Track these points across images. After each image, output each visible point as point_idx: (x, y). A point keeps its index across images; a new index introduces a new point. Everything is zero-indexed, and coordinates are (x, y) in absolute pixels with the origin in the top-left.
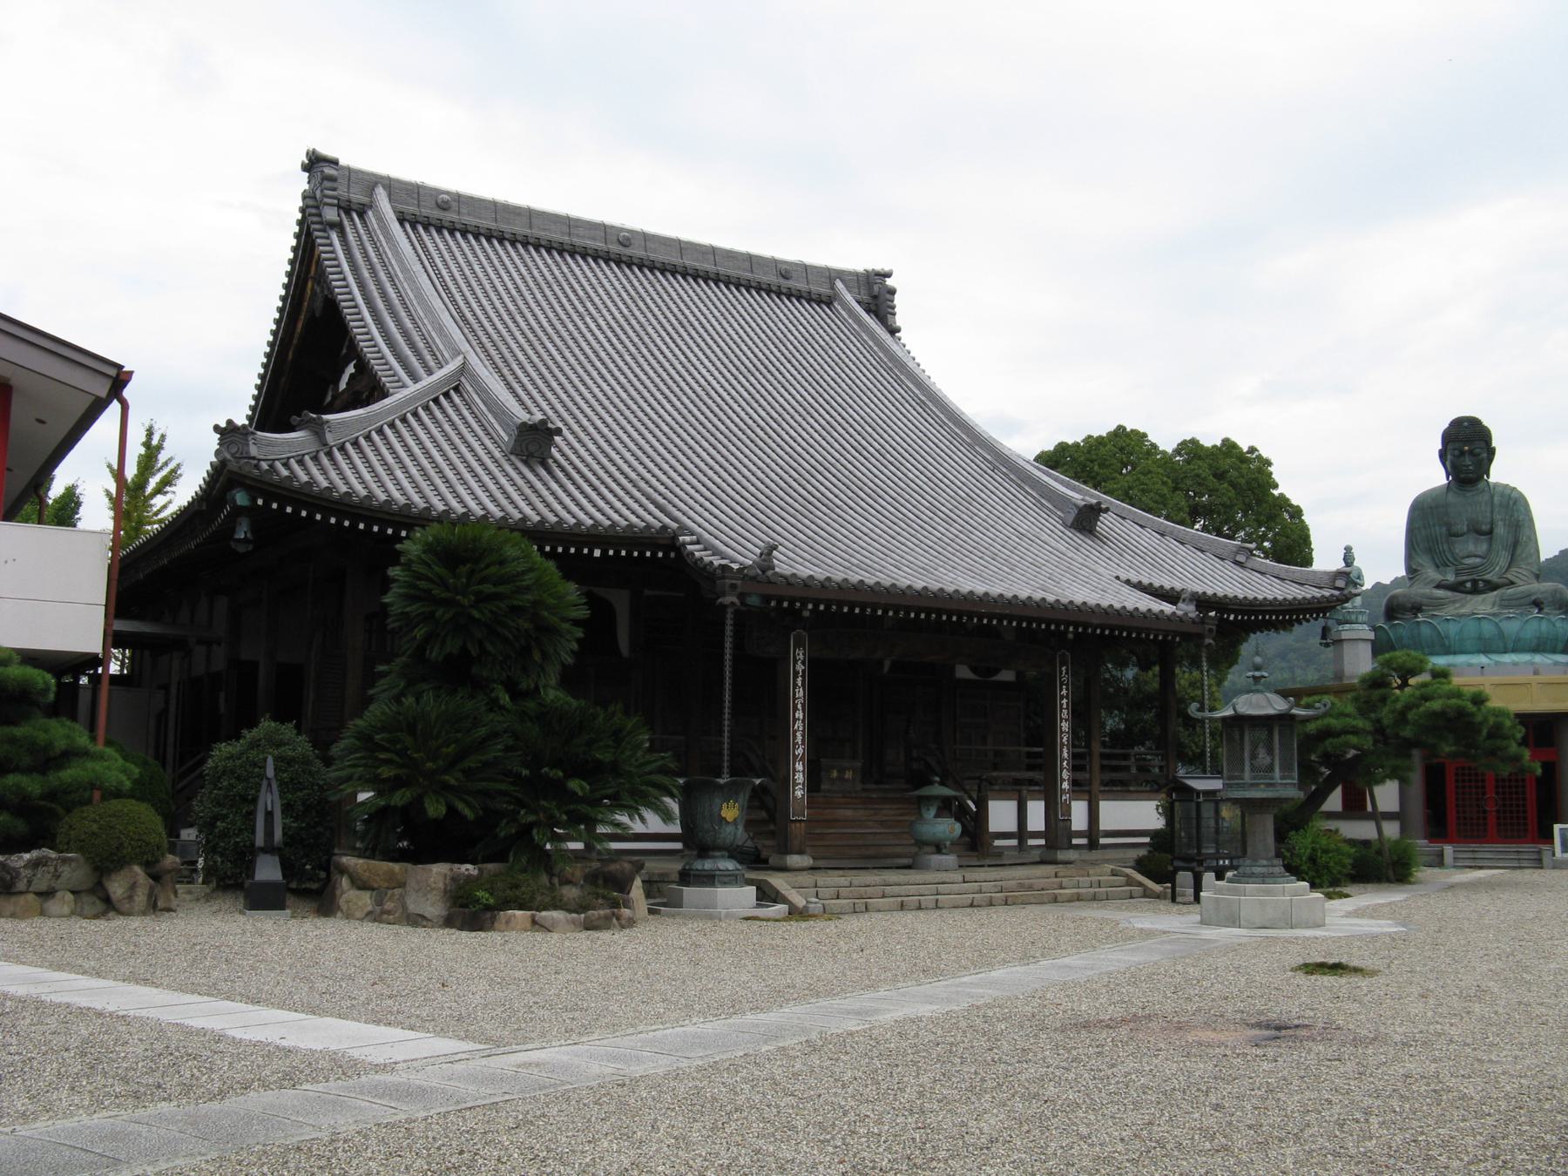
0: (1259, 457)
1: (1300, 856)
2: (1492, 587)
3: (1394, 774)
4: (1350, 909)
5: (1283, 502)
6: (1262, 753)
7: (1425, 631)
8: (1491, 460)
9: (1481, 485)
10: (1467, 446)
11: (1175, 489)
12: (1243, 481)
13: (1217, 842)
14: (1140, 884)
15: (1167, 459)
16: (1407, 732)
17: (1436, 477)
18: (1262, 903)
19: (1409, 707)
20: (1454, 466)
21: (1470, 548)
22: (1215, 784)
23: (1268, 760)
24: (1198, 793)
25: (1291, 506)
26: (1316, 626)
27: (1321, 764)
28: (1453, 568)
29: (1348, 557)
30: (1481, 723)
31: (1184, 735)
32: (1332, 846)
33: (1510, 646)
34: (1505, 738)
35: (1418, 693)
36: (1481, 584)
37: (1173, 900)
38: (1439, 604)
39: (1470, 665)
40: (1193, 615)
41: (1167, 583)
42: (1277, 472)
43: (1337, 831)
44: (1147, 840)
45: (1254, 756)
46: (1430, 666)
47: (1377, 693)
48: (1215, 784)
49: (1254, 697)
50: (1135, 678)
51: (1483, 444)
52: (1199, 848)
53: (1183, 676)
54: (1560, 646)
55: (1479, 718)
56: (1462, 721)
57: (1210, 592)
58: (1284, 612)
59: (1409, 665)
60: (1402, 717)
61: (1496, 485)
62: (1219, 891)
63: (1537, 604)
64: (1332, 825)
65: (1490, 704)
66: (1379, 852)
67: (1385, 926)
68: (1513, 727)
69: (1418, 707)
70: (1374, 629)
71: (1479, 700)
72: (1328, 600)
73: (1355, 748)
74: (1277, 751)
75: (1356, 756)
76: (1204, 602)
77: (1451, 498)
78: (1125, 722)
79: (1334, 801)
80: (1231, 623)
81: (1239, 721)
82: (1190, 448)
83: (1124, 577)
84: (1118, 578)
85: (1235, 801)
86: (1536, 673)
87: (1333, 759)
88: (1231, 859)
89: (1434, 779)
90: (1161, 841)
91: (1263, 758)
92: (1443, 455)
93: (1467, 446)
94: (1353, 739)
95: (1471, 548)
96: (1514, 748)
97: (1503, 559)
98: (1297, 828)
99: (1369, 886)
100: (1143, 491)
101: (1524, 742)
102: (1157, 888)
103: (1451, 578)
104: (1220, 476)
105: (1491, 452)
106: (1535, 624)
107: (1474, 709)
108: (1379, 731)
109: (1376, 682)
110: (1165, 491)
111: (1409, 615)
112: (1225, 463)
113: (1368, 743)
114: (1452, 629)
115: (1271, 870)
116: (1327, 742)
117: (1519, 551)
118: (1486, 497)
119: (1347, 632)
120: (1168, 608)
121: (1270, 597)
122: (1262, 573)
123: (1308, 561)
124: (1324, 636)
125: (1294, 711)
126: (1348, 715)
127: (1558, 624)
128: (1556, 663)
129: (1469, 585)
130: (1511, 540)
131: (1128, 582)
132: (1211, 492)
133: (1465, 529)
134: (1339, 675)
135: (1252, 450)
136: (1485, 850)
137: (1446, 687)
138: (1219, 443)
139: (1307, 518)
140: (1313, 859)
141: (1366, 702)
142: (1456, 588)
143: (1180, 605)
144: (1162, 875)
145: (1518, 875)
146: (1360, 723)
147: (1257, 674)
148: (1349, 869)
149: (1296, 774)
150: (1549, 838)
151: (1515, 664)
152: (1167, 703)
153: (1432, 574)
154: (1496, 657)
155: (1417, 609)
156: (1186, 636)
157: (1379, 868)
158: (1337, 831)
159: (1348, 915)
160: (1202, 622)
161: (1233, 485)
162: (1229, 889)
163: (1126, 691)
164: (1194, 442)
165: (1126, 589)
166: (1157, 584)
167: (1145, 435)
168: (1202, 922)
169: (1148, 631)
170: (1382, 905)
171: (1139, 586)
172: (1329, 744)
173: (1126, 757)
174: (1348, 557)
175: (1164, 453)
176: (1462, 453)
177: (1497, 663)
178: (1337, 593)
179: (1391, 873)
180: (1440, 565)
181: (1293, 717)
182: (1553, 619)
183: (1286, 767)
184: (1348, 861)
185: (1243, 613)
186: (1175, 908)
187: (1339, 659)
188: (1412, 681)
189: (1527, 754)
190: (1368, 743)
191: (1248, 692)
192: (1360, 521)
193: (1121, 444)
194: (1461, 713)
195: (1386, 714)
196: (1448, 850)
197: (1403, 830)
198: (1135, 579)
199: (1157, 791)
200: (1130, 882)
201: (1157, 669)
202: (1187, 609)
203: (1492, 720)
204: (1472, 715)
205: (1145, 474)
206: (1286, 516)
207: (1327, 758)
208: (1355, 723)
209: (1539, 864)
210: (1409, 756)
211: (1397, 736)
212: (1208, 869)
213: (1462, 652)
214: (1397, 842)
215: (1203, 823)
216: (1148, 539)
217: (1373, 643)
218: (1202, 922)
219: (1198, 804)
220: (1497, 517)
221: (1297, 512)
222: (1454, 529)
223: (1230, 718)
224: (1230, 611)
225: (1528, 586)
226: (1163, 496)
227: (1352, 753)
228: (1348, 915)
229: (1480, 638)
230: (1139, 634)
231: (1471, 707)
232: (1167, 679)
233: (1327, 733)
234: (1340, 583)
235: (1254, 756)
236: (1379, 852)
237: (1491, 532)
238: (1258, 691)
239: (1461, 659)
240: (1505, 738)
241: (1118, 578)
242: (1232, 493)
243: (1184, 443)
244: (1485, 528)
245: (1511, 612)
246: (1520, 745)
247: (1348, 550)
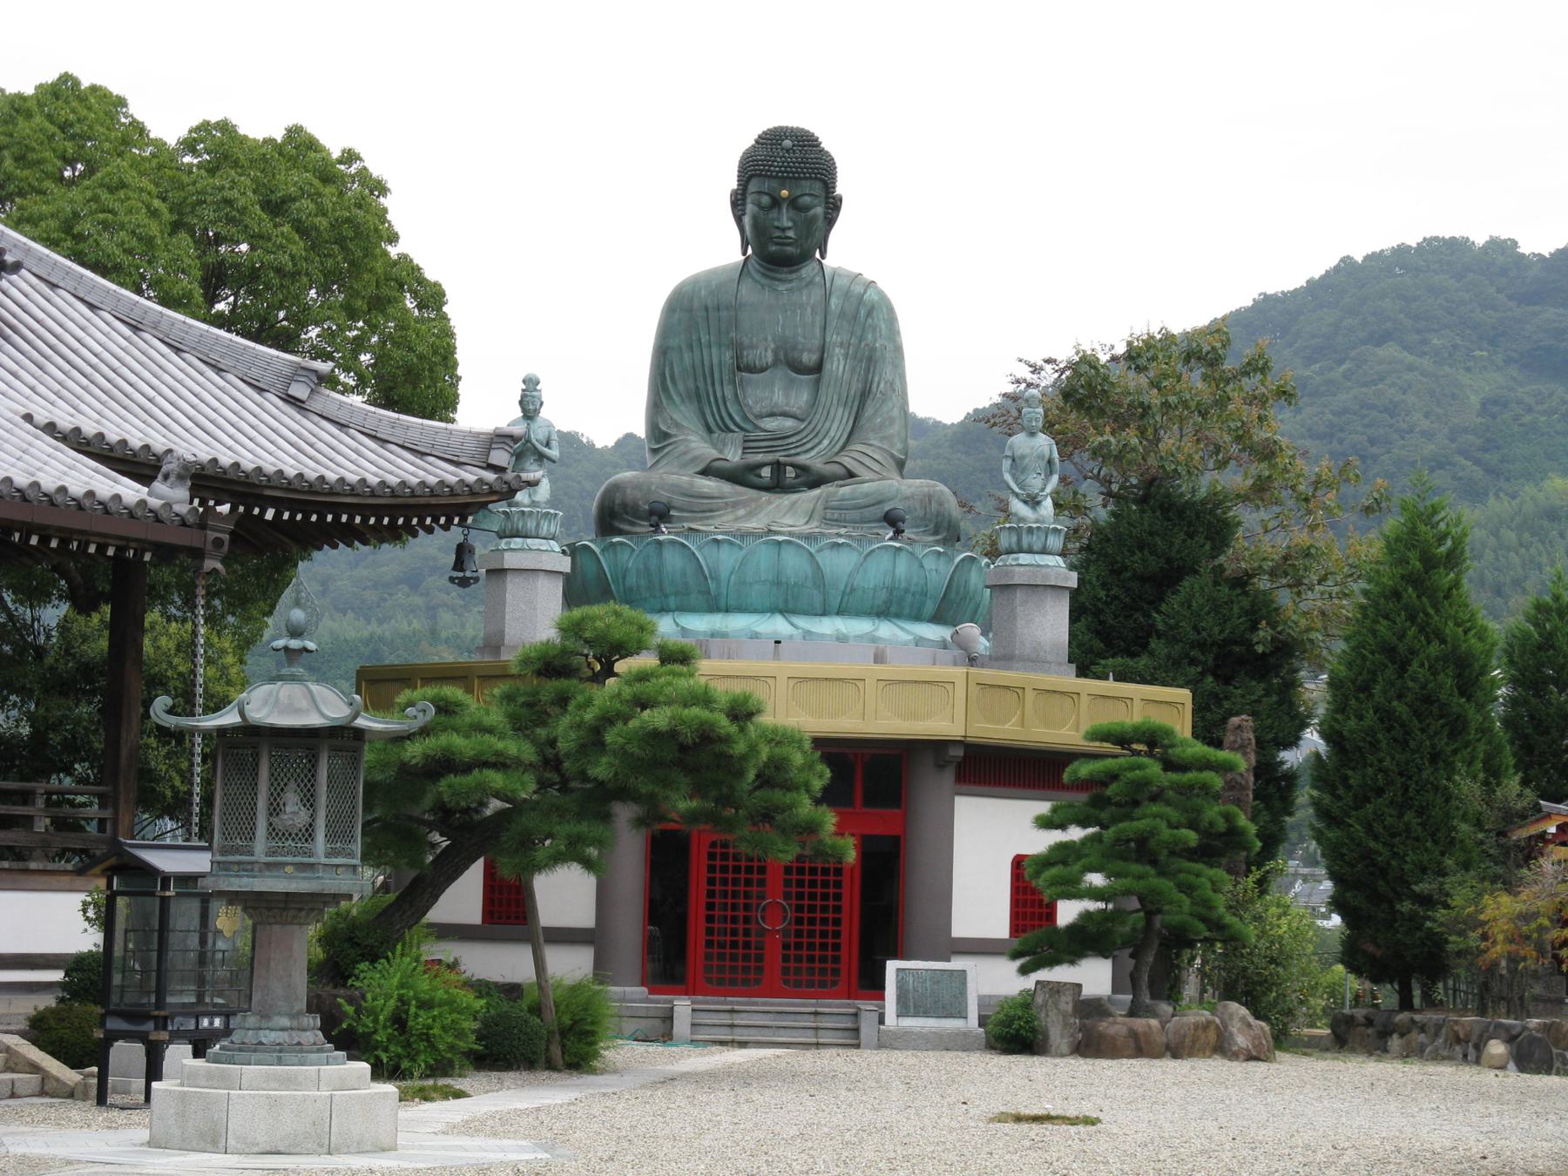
0: (364, 174)
1: (373, 1013)
2: (816, 481)
3: (573, 853)
4: (458, 1119)
5: (407, 276)
6: (292, 801)
7: (673, 561)
8: (830, 222)
9: (808, 271)
10: (787, 188)
11: (176, 227)
12: (322, 222)
13: (201, 981)
14: (35, 1068)
15: (163, 157)
16: (601, 769)
17: (719, 246)
18: (274, 1103)
19: (607, 720)
20: (756, 225)
21: (775, 398)
22: (198, 862)
23: (303, 817)
24: (166, 879)
25: (422, 281)
26: (436, 546)
27: (432, 826)
28: (739, 435)
29: (530, 405)
30: (744, 758)
31: (157, 758)
32: (440, 994)
33: (835, 603)
34: (789, 787)
35: (627, 692)
36: (790, 473)
37: (101, 1100)
38: (705, 507)
39: (755, 636)
40: (183, 509)
41: (135, 433)
42: (398, 209)
43: (453, 966)
44: (57, 976)
45: (275, 809)
46: (656, 641)
47: (552, 686)
48: (198, 862)
49: (285, 691)
50: (64, 627)
51: (817, 188)
52: (160, 993)
53: (162, 632)
54: (930, 607)
55: (740, 747)
56: (705, 755)
57: (226, 460)
58: (378, 510)
59: (617, 634)
60: (594, 739)
61: (835, 273)
62: (190, 1078)
63: (893, 521)
64: (447, 951)
65: (766, 719)
66: (536, 1010)
67: (517, 1151)
68: (809, 766)
69: (626, 720)
70: (573, 551)
71: (742, 712)
72: (471, 490)
73: (497, 795)
74: (322, 800)
75: (500, 814)
76: (208, 481)
77: (748, 292)
78: (32, 719)
79: (463, 898)
80: (268, 529)
81: (252, 736)
82: (218, 143)
83: (42, 417)
84: (28, 418)
85: (233, 898)
86: (879, 658)
87: (428, 819)
88: (227, 1016)
89: (667, 854)
90: (86, 977)
91: (294, 812)
92: (738, 202)
93: (787, 188)
94: (496, 779)
95: (778, 397)
96: (805, 808)
97: (837, 427)
98: (373, 958)
99: (509, 1077)
100: (106, 226)
101: (828, 797)
102: (70, 1076)
103: (734, 456)
104: (275, 207)
105: (833, 206)
106: (885, 560)
107: (733, 729)
108: (550, 762)
109: (551, 665)
110: (154, 229)
111: (643, 527)
112: (290, 181)
113: (526, 788)
114: (727, 560)
115: (297, 1037)
116: (443, 784)
117: (869, 411)
118: (816, 295)
119: (516, 554)
120: (130, 491)
121: (353, 478)
122: (342, 426)
123: (441, 404)
124: (459, 565)
125: (361, 722)
126: (489, 730)
127: (930, 564)
128: (919, 641)
129: (766, 472)
130: (856, 386)
131: (50, 428)
132: (255, 240)
133: (770, 357)
134: (494, 644)
135: (350, 157)
136: (755, 1010)
137: (683, 683)
138: (279, 136)
139: (452, 309)
140: (399, 1021)
141: (530, 705)
142: (740, 476)
143: (158, 485)
144: (84, 1051)
145: (807, 1060)
146: (512, 747)
147: (295, 644)
148: (471, 1043)
149: (357, 847)
150: (874, 986)
151: (841, 639)
152: (118, 678)
153: (700, 446)
154: (804, 622)
155: (660, 515)
156: (167, 553)
157: (533, 1039)
158: (453, 966)
159: (451, 1129)
160: (202, 525)
161: (301, 229)
162: (210, 1076)
163: (40, 652)
164: (225, 127)
165: (46, 444)
166: (113, 436)
167: (121, 102)
168: (153, 1143)
169: (85, 537)
170: (520, 1113)
171: (76, 441)
172: (448, 785)
173: (26, 797)
174: (530, 405)
175: (160, 144)
176: (776, 202)
177: (807, 634)
178: (490, 476)
179: (556, 1051)
180: (716, 426)
181: (359, 734)
182: (920, 551)
183: (336, 833)
184: (469, 1025)
185: (294, 506)
186: (102, 1115)
187: (496, 611)
188: (621, 666)
189: (829, 819)
190: (526, 788)
191: (273, 680)
192: (557, 328)
193: (65, 114)
194: (707, 736)
195: (564, 730)
196: (683, 1007)
197: (599, 964)
198: (65, 423)
199: (80, 872)
200: (14, 1063)
201: (107, 609)
202: (171, 496)
203: (765, 752)
204: (727, 740)
205: (112, 190)
206: (410, 303)
207: (446, 817)
208: (500, 745)
209: (852, 1038)
210: (606, 818)
211: (583, 776)
212: (177, 1036)
213: (742, 609)
214: (575, 989)
215: (174, 939)
216: (103, 336)
217: (568, 580)
218: (149, 1144)
219: (165, 901)
220: (833, 338)
221: (433, 297)
222: (750, 356)
223: (234, 729)
224: (265, 502)
225: (881, 484)
226: (149, 242)
227: (495, 805)
228: (451, 1129)
229: (777, 583)
230: (64, 542)
231: (725, 725)
232: (126, 631)
233: (445, 765)
234: (500, 457)
235: (275, 809)
236: (536, 1010)
237: (818, 368)
238: (293, 679)
239: (737, 623)
240: (789, 787)
241: (28, 418)
242: (299, 247)
243: (205, 126)
244: (809, 358)
245: (839, 534)
246: (818, 802)
247: (531, 384)
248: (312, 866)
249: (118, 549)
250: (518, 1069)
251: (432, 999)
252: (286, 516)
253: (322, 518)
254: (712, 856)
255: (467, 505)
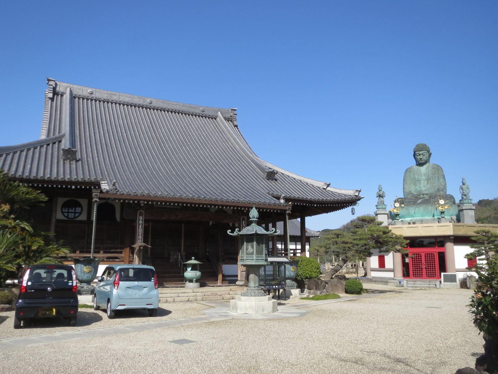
45: (247, 249)
224: (314, 204)
235: (247, 249)
248: (243, 259)
249: (262, 210)
250: (200, 277)
251: (15, 177)
252: (318, 205)
253: (325, 205)
254: (435, 275)
255: (352, 202)
